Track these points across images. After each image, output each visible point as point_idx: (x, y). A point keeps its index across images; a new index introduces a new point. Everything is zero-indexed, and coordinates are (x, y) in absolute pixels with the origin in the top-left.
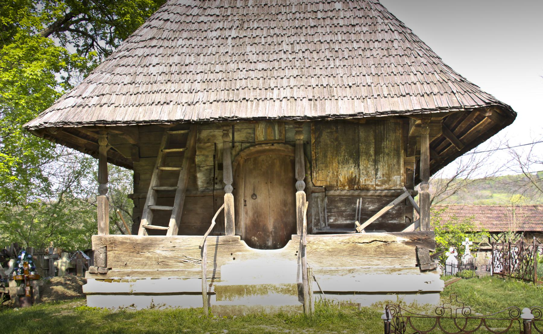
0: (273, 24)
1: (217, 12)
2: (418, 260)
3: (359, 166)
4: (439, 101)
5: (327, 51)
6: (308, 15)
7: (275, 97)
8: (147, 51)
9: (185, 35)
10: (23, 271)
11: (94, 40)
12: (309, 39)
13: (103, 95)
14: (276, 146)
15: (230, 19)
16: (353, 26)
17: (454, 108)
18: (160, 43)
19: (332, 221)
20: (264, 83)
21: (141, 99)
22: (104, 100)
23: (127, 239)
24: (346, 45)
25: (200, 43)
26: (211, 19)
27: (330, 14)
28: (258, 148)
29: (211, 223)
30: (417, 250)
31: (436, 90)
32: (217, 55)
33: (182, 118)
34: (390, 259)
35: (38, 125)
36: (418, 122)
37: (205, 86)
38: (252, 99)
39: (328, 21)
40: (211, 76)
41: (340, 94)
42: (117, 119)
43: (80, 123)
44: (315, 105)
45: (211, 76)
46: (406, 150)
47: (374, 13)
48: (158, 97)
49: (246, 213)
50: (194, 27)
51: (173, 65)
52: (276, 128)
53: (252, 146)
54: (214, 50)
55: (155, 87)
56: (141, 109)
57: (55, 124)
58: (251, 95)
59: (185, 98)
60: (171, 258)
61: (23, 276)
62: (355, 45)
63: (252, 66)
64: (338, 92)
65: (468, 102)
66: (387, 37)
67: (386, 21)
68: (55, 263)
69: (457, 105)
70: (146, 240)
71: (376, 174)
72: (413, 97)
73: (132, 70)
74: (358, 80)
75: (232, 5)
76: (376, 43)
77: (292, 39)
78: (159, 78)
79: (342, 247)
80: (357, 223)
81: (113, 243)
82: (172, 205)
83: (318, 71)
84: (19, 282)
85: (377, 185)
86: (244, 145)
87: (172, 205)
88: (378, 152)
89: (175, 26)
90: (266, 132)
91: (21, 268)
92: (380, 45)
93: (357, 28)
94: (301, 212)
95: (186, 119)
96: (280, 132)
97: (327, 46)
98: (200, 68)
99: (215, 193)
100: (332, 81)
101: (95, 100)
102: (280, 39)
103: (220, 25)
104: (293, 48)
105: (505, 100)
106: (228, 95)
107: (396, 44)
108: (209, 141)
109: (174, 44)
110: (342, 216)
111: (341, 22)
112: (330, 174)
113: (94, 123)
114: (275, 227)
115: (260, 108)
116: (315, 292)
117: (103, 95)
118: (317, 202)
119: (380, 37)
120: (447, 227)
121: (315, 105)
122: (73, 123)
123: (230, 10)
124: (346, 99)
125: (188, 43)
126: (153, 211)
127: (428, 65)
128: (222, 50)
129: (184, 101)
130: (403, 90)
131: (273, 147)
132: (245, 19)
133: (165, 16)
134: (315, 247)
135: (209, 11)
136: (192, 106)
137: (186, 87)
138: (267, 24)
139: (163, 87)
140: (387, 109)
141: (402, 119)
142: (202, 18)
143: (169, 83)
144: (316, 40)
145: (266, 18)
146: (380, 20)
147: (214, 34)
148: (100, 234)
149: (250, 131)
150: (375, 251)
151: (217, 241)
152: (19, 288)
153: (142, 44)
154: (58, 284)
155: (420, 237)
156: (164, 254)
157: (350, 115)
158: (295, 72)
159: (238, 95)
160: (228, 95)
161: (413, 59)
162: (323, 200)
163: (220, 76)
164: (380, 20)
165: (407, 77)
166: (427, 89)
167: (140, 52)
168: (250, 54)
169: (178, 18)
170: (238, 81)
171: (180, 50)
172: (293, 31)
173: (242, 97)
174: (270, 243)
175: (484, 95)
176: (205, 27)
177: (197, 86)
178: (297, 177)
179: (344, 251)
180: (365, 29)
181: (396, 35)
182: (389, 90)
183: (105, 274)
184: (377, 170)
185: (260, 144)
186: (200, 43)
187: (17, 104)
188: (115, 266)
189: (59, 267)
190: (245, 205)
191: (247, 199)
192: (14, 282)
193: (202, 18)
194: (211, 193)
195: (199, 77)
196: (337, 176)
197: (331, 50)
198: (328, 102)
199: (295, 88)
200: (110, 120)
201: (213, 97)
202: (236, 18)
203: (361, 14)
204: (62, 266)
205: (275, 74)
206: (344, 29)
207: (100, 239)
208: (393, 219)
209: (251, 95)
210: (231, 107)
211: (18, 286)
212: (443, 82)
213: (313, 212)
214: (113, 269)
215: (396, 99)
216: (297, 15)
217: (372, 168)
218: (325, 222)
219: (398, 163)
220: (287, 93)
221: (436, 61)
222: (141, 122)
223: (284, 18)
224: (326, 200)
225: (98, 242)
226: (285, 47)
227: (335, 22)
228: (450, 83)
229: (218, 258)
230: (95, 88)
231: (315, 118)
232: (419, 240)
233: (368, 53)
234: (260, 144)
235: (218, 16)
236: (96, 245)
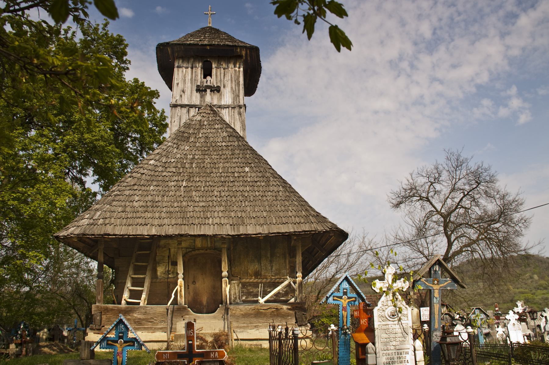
0: (208, 179)
1: (174, 170)
2: (296, 319)
3: (261, 264)
4: (304, 227)
5: (241, 197)
6: (230, 174)
7: (210, 223)
8: (131, 192)
9: (155, 183)
10: (21, 336)
11: (69, 171)
12: (230, 189)
13: (106, 218)
14: (208, 251)
15: (182, 175)
16: (256, 182)
17: (312, 231)
18: (140, 188)
19: (244, 298)
20: (204, 214)
21: (131, 221)
22: (107, 221)
23: (115, 307)
24: (252, 193)
25: (164, 189)
26: (170, 174)
27: (242, 174)
28: (197, 252)
29: (171, 297)
30: (295, 313)
31: (302, 221)
32: (175, 197)
33: (156, 234)
34: (280, 319)
35: (66, 235)
36: (295, 238)
37: (168, 215)
38: (197, 223)
39: (241, 179)
40: (172, 209)
41: (248, 222)
42: (116, 233)
43: (93, 235)
44: (234, 228)
45: (172, 209)
46: (290, 254)
47: (268, 175)
48: (140, 221)
49: (189, 293)
50: (160, 178)
51: (148, 202)
52: (209, 240)
53: (193, 250)
54: (173, 193)
55: (138, 215)
56: (130, 228)
57: (78, 235)
58: (197, 221)
59: (156, 222)
60: (144, 319)
61: (21, 340)
62: (257, 193)
63: (196, 204)
64: (247, 221)
65: (320, 228)
66: (276, 189)
67: (275, 180)
68: (38, 333)
69: (313, 229)
70: (128, 308)
71: (272, 269)
72: (290, 225)
73: (123, 204)
74: (258, 214)
75: (183, 166)
76: (269, 192)
77: (220, 189)
78: (140, 209)
79: (251, 312)
80: (259, 298)
81: (107, 310)
82: (143, 287)
83: (235, 208)
84: (17, 345)
85: (272, 276)
86: (188, 250)
87: (143, 287)
88: (272, 256)
89: (148, 178)
90: (202, 242)
91: (20, 334)
92: (271, 194)
93: (258, 183)
94: (225, 291)
95: (158, 234)
96: (211, 242)
97: (241, 194)
98: (165, 204)
99: (169, 280)
100: (244, 215)
101: (101, 221)
102: (212, 189)
103: (176, 178)
104: (220, 194)
105: (341, 226)
106: (183, 221)
107: (281, 193)
108: (165, 247)
109: (148, 189)
110: (251, 295)
111: (249, 180)
112: (243, 269)
113: (102, 235)
114: (207, 303)
115: (202, 229)
116: (235, 340)
117: (106, 218)
118: (235, 286)
119: (271, 189)
120: (331, 311)
121: (234, 228)
122: (89, 235)
123: (181, 169)
124: (251, 225)
125: (157, 188)
126: (130, 290)
127: (299, 206)
128: (178, 193)
129: (156, 224)
130: (284, 220)
131: (206, 252)
132: (191, 175)
133: (142, 171)
134: (234, 312)
135: (168, 169)
136: (161, 227)
137: (157, 215)
138: (204, 179)
139: (143, 215)
140: (275, 231)
141: (287, 237)
142: (164, 174)
143: (147, 213)
144: (234, 190)
145: (204, 175)
146: (272, 179)
147: (173, 183)
148: (97, 304)
149: (192, 241)
150: (271, 314)
151: (173, 309)
152: (17, 349)
153: (128, 188)
154: (44, 347)
155: (297, 305)
156: (139, 316)
157: (254, 234)
158: (222, 208)
159: (188, 221)
160: (183, 221)
161: (290, 203)
162: (238, 286)
163: (177, 209)
164: (272, 179)
165: (287, 213)
166: (297, 220)
167: (127, 193)
168: (195, 197)
169: (150, 173)
170: (188, 213)
171: (152, 193)
172: (221, 184)
173: (191, 222)
174: (205, 311)
175: (329, 224)
176: (167, 179)
177: (163, 215)
178: (223, 269)
179: (252, 314)
180: (263, 184)
181: (281, 188)
182: (277, 221)
183: (100, 329)
184: (272, 267)
185: (198, 249)
186: (164, 189)
187: (46, 221)
188: (107, 325)
189: (41, 336)
190: (188, 288)
191: (190, 284)
192: (13, 344)
193: (164, 174)
194: (166, 280)
195: (164, 210)
196: (247, 270)
197: (243, 196)
198: (241, 227)
199: (222, 218)
200: (112, 234)
201: (173, 222)
202: (186, 174)
203: (260, 175)
204: (43, 335)
205: (210, 209)
206: (251, 184)
207: (98, 307)
208: (283, 297)
209: (197, 221)
210: (185, 228)
211: (17, 347)
212: (307, 216)
213: (232, 293)
214: (105, 327)
215: (280, 225)
216: (223, 174)
217: (269, 265)
218: (240, 299)
219: (285, 262)
220: (217, 221)
221: (303, 203)
222: (131, 235)
223: (215, 175)
224: (240, 285)
225: (95, 309)
226: (216, 193)
227: (245, 179)
228: (311, 217)
229: (174, 319)
230: (101, 214)
231: (233, 235)
232: (297, 307)
233: (265, 198)
234: (198, 249)
235: (174, 173)
236: (95, 311)
